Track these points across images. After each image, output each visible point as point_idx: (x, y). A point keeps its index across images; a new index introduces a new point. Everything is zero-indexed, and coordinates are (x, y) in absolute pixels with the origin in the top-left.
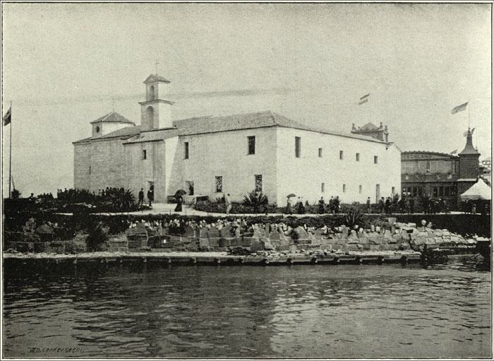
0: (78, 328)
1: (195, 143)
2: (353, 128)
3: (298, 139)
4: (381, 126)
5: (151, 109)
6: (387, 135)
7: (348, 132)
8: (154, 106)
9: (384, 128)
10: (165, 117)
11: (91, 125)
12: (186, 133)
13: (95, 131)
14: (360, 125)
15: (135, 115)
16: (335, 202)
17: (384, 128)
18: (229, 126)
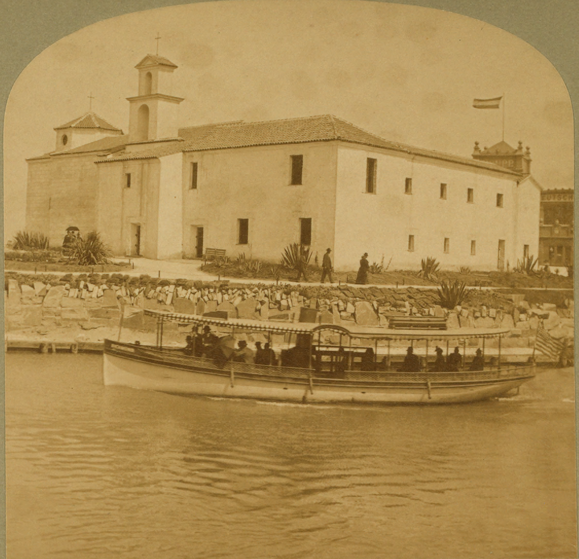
0: (179, 488)
1: (205, 161)
2: (476, 149)
3: (371, 163)
4: (520, 148)
5: (145, 109)
6: (528, 162)
7: (467, 154)
8: (149, 103)
9: (524, 150)
10: (167, 120)
11: (55, 133)
12: (195, 147)
13: (60, 140)
14: (488, 142)
15: (122, 118)
16: (429, 266)
17: (524, 150)
18: (309, 135)
